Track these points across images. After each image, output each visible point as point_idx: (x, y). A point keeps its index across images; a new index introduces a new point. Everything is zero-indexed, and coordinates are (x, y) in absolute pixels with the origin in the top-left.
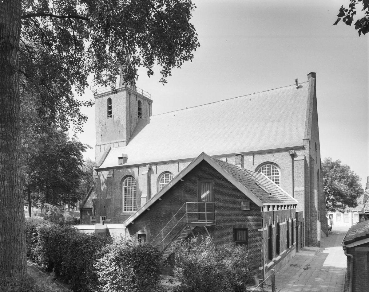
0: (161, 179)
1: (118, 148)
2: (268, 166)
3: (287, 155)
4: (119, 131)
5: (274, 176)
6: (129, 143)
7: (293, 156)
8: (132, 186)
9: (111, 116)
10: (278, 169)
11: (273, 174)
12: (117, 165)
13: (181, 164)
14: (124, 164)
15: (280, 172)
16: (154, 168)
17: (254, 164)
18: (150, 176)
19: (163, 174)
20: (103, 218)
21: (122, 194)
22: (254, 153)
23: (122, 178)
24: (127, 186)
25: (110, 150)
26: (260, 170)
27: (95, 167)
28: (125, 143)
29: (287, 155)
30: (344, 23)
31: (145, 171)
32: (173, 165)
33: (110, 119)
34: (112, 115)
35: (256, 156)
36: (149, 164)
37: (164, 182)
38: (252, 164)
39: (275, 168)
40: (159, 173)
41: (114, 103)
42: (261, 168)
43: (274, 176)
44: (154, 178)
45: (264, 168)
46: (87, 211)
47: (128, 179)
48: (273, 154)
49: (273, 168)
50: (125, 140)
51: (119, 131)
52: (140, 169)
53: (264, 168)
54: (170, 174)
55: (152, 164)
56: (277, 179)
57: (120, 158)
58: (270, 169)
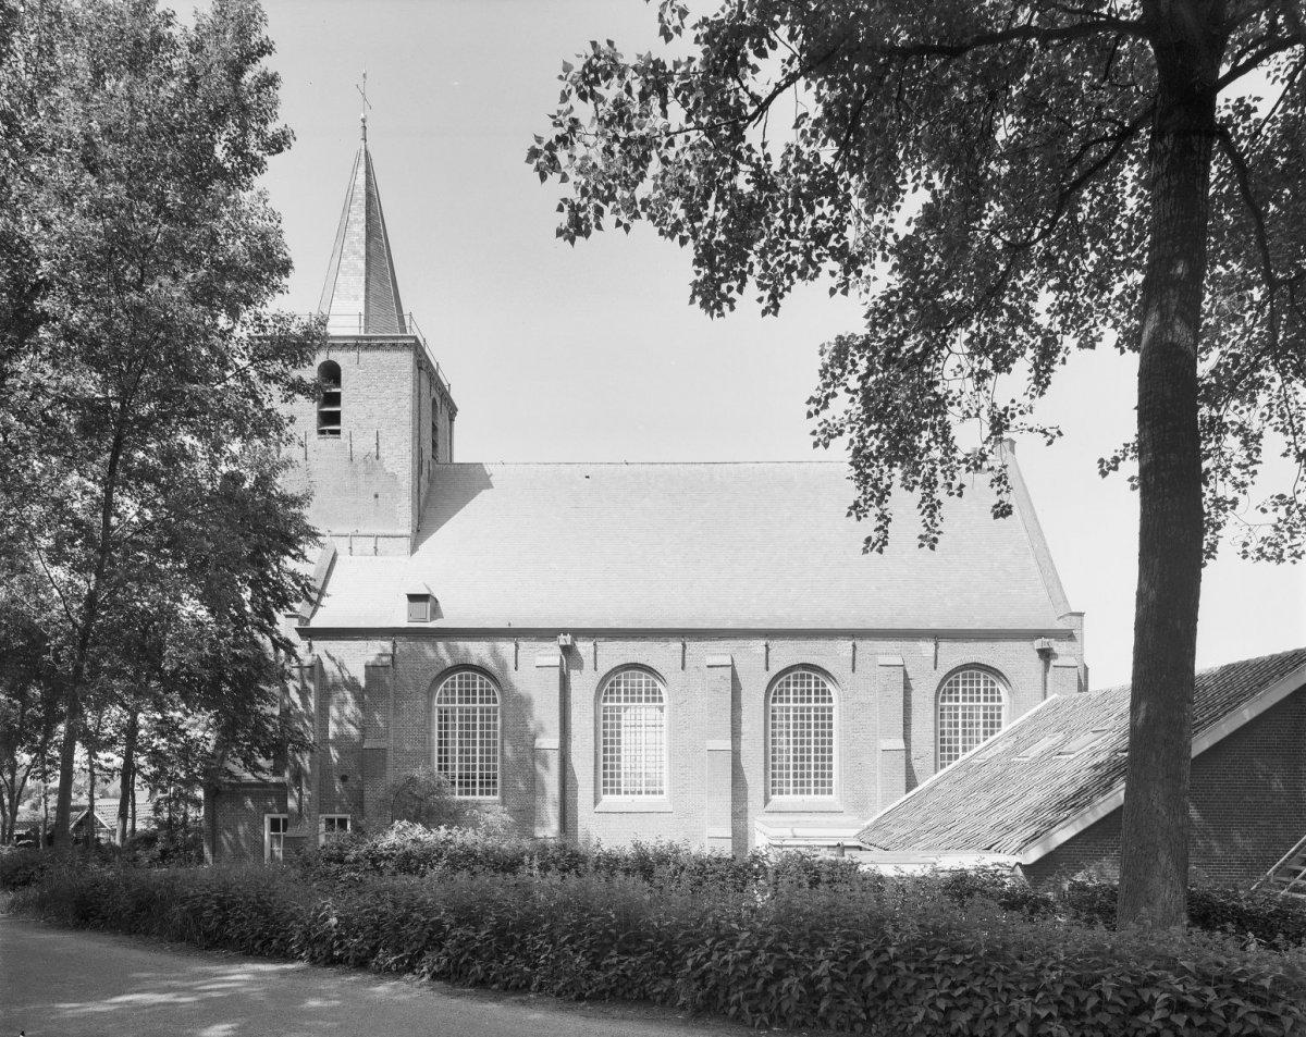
0: (607, 686)
1: (374, 557)
2: (972, 676)
3: (1028, 652)
4: (376, 496)
5: (989, 704)
6: (422, 547)
7: (1046, 654)
8: (457, 704)
9: (338, 432)
10: (829, 686)
11: (481, 701)
12: (403, 623)
13: (775, 645)
14: (432, 619)
15: (834, 695)
16: (584, 647)
17: (687, 665)
18: (568, 672)
19: (616, 673)
20: (330, 822)
21: (429, 733)
22: (937, 636)
23: (435, 673)
24: (478, 704)
25: (334, 560)
26: (612, 684)
27: (296, 620)
28: (406, 543)
29: (1028, 652)
30: (277, 156)
31: (550, 654)
32: (663, 644)
33: (331, 441)
34: (343, 427)
35: (943, 645)
36: (565, 631)
37: (619, 700)
38: (764, 665)
39: (993, 683)
40: (604, 668)
41: (355, 385)
42: (614, 679)
43: (989, 704)
44: (583, 685)
45: (792, 681)
46: (246, 794)
47: (460, 677)
48: (991, 644)
49: (986, 683)
50: (408, 531)
51: (376, 496)
52: (521, 649)
53: (792, 681)
54: (813, 675)
55: (578, 633)
56: (996, 712)
57: (413, 598)
58: (978, 683)
